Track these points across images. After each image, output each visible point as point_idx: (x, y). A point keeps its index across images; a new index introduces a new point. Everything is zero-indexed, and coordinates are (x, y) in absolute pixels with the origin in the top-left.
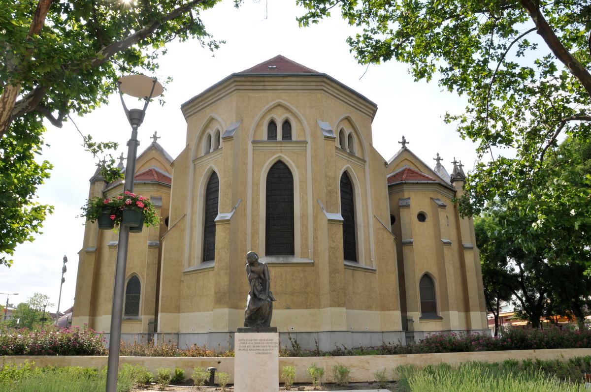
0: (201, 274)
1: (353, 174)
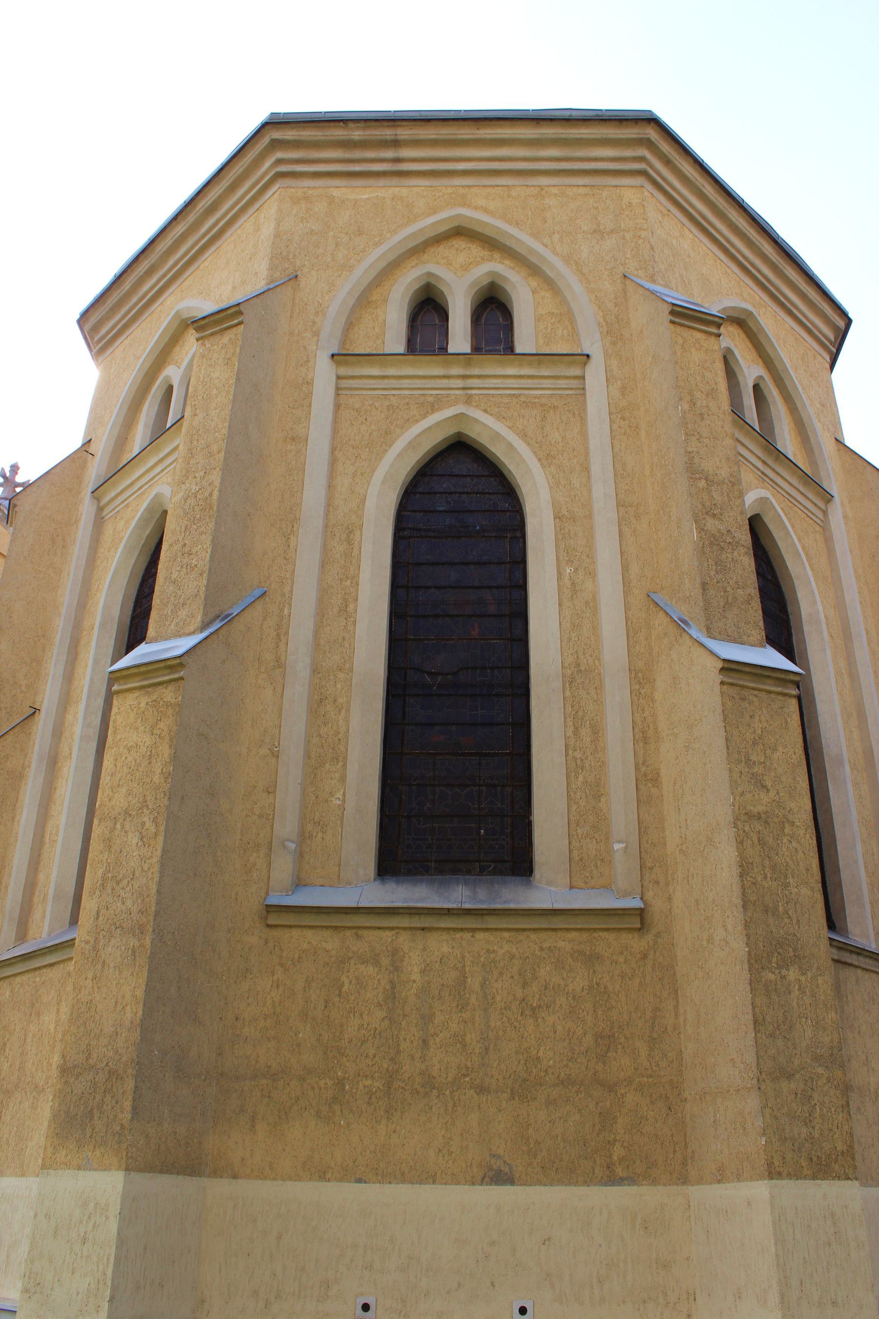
0: (50, 974)
1: (788, 534)
